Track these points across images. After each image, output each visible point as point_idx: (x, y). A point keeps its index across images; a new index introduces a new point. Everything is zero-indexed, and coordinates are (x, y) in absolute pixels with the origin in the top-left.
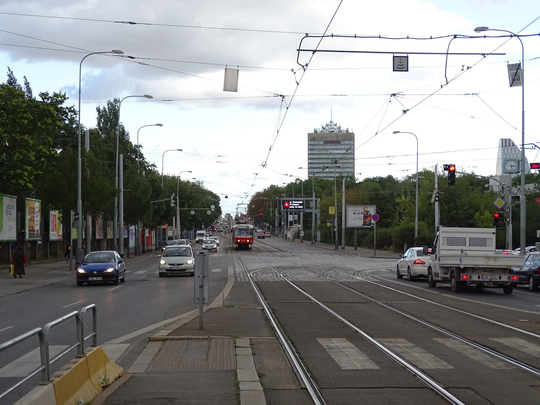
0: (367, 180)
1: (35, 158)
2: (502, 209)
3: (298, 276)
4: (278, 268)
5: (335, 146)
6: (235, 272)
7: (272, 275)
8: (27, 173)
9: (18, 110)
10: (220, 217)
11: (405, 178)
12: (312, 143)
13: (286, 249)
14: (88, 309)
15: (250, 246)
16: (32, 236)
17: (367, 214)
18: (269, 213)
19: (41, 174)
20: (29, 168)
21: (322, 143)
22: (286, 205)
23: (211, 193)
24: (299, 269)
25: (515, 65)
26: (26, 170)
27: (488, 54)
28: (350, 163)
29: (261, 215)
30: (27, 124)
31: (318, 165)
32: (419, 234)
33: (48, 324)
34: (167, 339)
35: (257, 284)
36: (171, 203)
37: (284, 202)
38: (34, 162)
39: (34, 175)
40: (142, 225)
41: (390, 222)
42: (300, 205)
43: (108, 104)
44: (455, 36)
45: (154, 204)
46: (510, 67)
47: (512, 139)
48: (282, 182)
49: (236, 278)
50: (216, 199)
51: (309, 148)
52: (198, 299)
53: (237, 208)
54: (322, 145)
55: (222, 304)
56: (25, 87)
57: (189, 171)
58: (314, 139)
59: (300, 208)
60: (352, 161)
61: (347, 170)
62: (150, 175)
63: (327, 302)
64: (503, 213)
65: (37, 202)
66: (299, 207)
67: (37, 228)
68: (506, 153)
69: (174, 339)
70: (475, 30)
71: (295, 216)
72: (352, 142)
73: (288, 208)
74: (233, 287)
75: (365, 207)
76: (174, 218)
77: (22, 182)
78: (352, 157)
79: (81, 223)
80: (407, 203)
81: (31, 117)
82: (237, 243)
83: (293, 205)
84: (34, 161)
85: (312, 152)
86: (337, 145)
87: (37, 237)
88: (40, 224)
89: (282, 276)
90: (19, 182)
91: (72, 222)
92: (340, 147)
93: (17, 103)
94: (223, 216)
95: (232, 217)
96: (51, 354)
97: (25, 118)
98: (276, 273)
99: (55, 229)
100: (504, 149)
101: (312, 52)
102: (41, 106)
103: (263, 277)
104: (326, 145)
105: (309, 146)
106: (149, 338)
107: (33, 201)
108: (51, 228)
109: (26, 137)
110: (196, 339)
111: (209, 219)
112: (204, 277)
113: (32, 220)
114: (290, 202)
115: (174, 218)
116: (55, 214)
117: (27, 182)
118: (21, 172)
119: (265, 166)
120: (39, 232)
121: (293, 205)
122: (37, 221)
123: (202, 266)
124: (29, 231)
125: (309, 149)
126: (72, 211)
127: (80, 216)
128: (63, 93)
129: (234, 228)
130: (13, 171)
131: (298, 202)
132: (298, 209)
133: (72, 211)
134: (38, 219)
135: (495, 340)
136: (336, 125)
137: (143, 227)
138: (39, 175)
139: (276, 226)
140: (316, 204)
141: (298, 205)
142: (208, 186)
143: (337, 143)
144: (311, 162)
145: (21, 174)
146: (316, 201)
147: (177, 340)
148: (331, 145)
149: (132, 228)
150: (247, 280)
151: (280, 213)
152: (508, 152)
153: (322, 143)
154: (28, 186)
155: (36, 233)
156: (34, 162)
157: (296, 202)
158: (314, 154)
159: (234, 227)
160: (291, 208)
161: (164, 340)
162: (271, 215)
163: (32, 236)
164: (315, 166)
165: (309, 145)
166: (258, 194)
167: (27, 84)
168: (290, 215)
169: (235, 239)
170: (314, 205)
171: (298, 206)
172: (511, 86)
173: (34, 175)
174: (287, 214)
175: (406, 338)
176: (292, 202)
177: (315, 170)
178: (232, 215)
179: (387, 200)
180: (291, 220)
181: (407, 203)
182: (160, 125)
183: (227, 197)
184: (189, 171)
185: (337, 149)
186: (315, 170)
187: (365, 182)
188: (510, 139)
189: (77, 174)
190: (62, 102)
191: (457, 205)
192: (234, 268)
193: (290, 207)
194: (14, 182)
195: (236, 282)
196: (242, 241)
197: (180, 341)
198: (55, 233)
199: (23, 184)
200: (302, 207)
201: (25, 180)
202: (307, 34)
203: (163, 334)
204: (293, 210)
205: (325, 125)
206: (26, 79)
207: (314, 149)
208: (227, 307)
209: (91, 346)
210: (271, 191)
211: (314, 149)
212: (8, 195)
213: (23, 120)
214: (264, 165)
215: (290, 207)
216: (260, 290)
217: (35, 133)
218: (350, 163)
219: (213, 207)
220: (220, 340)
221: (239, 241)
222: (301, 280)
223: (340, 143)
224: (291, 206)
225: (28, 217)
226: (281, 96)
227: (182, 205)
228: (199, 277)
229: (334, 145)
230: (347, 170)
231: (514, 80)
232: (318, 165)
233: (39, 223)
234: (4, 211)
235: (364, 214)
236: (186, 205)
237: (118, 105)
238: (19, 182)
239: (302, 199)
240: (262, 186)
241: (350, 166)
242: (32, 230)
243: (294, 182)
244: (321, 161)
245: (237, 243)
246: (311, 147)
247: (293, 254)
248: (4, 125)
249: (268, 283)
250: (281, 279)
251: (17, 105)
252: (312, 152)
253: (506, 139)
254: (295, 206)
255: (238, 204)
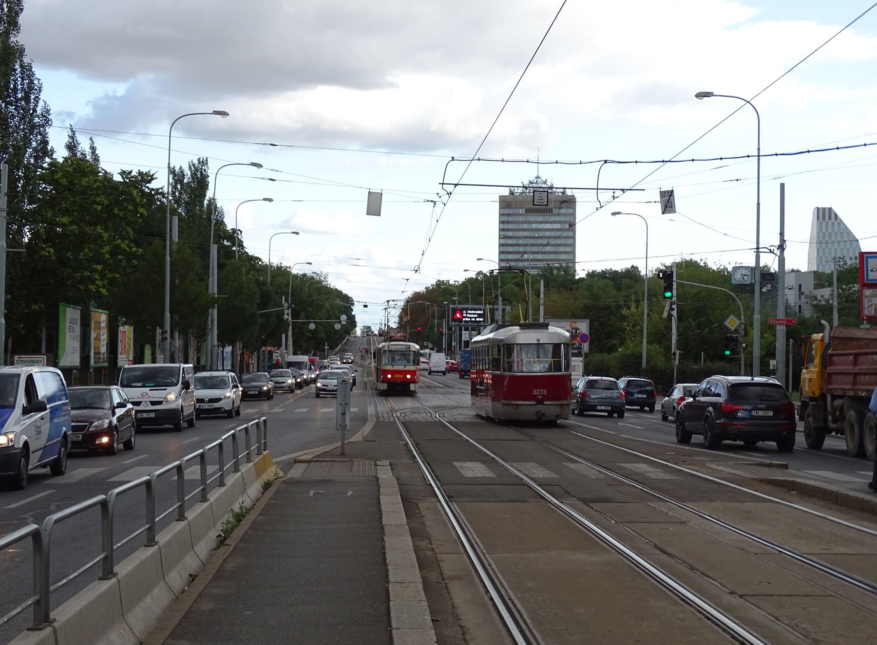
0: (592, 275)
1: (110, 255)
2: (736, 330)
3: (458, 417)
4: (434, 407)
5: (544, 217)
6: (377, 412)
7: (425, 415)
8: (97, 275)
9: (89, 192)
10: (354, 331)
11: (654, 272)
12: (507, 211)
13: (453, 384)
14: (252, 425)
15: (412, 387)
16: (97, 360)
17: (576, 332)
18: (432, 327)
19: (117, 277)
20: (99, 267)
21: (522, 211)
22: (458, 315)
23: (339, 294)
24: (463, 409)
25: (668, 192)
26: (96, 271)
27: (627, 190)
28: (567, 245)
29: (419, 331)
30: (100, 210)
31: (516, 249)
32: (647, 363)
33: (51, 516)
34: (312, 461)
35: (404, 424)
36: (284, 314)
37: (455, 311)
38: (109, 262)
39: (107, 279)
40: (241, 346)
41: (614, 345)
42: (480, 316)
43: (190, 168)
44: (606, 162)
45: (261, 315)
46: (663, 194)
47: (834, 208)
48: (456, 276)
49: (378, 418)
50: (346, 303)
51: (501, 220)
52: (340, 425)
53: (386, 309)
54: (522, 215)
55: (362, 439)
56: (90, 152)
57: (307, 263)
58: (509, 206)
59: (480, 322)
60: (570, 241)
61: (563, 257)
62: (252, 272)
63: (479, 439)
64: (737, 337)
65: (103, 314)
66: (477, 320)
67: (103, 349)
68: (824, 230)
69: (319, 461)
70: (696, 96)
71: (472, 332)
72: (571, 211)
73: (460, 320)
74: (374, 426)
75: (574, 322)
76: (284, 335)
77: (92, 287)
78: (572, 235)
79: (168, 344)
80: (638, 316)
81: (105, 201)
82: (385, 380)
83: (468, 315)
84: (108, 259)
85: (506, 226)
86: (547, 216)
87: (103, 362)
88: (107, 344)
89: (438, 417)
90: (89, 287)
91: (157, 342)
92: (552, 219)
93: (88, 183)
94: (358, 331)
95: (373, 332)
96: (208, 469)
97: (98, 203)
98: (431, 413)
99: (125, 352)
100: (821, 224)
101: (454, 186)
102: (121, 188)
103: (412, 417)
104: (529, 215)
105: (501, 217)
106: (295, 460)
107: (99, 312)
108: (119, 350)
109: (99, 229)
110: (339, 461)
111: (337, 337)
112: (346, 404)
113: (98, 339)
114: (465, 312)
115: (284, 335)
116: (126, 332)
117: (99, 287)
118: (89, 274)
119: (418, 272)
120: (105, 356)
121: (468, 315)
122: (104, 340)
123: (344, 393)
124: (95, 353)
125: (501, 222)
126: (158, 328)
127: (168, 335)
128: (152, 173)
129: (380, 349)
130: (79, 274)
131: (477, 312)
132: (476, 321)
133: (158, 328)
134: (104, 337)
135: (622, 465)
136: (545, 183)
137: (243, 349)
138: (114, 278)
139: (444, 347)
140: (503, 317)
141: (476, 316)
142: (334, 283)
143: (547, 212)
144: (503, 243)
145: (89, 277)
146: (504, 310)
147: (321, 461)
148: (537, 215)
149: (228, 349)
150: (392, 420)
151: (450, 329)
152: (827, 229)
153: (522, 211)
154: (101, 292)
155: (102, 356)
156: (109, 262)
157: (473, 312)
158: (509, 230)
159: (380, 346)
160: (465, 321)
161: (309, 462)
162: (435, 330)
163: (97, 360)
164: (511, 249)
165: (501, 215)
166: (417, 296)
167: (93, 149)
168: (465, 330)
169: (381, 373)
170: (500, 317)
171: (475, 318)
172: (663, 213)
173: (107, 279)
174: (460, 330)
175: (536, 463)
176: (466, 312)
177: (510, 257)
178: (373, 329)
179: (610, 311)
180: (466, 340)
181: (638, 316)
182: (270, 200)
183: (366, 306)
184: (307, 263)
185: (546, 222)
186: (510, 257)
187: (589, 278)
188: (830, 209)
189: (164, 278)
190: (150, 182)
191: (710, 320)
192: (376, 407)
193: (464, 319)
194: (82, 288)
195: (378, 422)
196: (396, 376)
197: (324, 463)
198: (124, 356)
199: (94, 290)
200: (482, 319)
201: (97, 285)
202: (453, 158)
203: (309, 457)
204: (470, 323)
205: (528, 182)
206: (92, 141)
207: (508, 222)
208: (367, 441)
209: (29, 629)
210: (437, 291)
211: (508, 222)
212: (72, 306)
213: (95, 206)
214: (416, 269)
215: (464, 319)
216: (407, 429)
217: (110, 222)
218: (567, 245)
219: (344, 318)
220: (361, 462)
221: (389, 376)
222: (461, 420)
223: (552, 212)
224: (465, 317)
225: (93, 335)
226: (432, 201)
227: (295, 315)
228: (341, 404)
229: (541, 216)
230: (563, 257)
231: (666, 207)
232: (516, 249)
233: (105, 342)
234: (67, 328)
235: (572, 332)
236: (302, 315)
237: (206, 168)
238: (89, 287)
239: (482, 307)
240: (423, 283)
241: (568, 249)
242: (97, 353)
243: (474, 277)
244: (521, 242)
245: (385, 380)
246: (505, 219)
247: (462, 391)
248: (69, 211)
249: (418, 424)
250: (436, 419)
251: (88, 186)
252: (506, 226)
253: (824, 209)
254: (471, 318)
255: (388, 301)
